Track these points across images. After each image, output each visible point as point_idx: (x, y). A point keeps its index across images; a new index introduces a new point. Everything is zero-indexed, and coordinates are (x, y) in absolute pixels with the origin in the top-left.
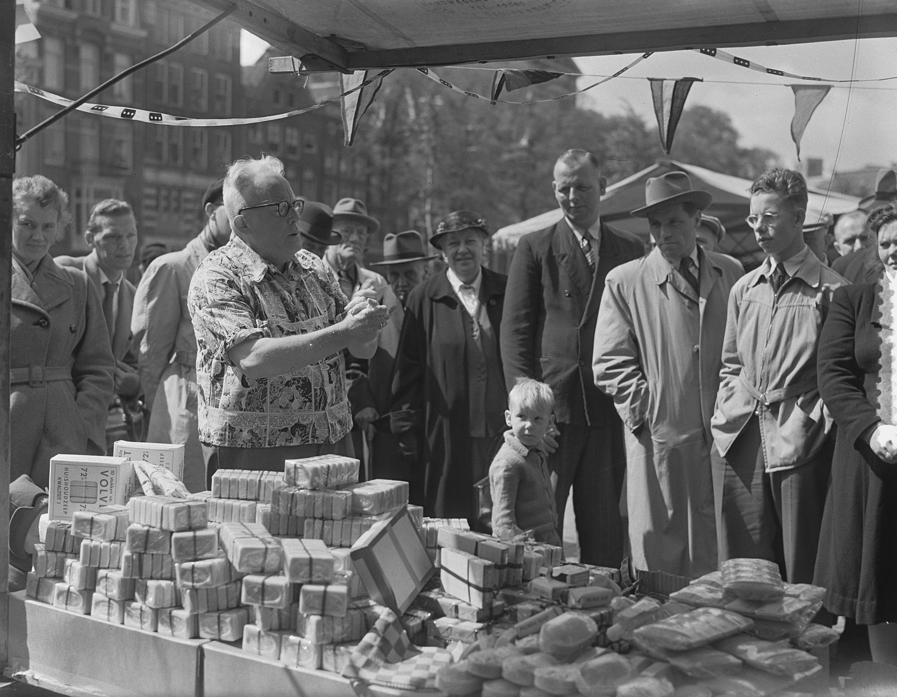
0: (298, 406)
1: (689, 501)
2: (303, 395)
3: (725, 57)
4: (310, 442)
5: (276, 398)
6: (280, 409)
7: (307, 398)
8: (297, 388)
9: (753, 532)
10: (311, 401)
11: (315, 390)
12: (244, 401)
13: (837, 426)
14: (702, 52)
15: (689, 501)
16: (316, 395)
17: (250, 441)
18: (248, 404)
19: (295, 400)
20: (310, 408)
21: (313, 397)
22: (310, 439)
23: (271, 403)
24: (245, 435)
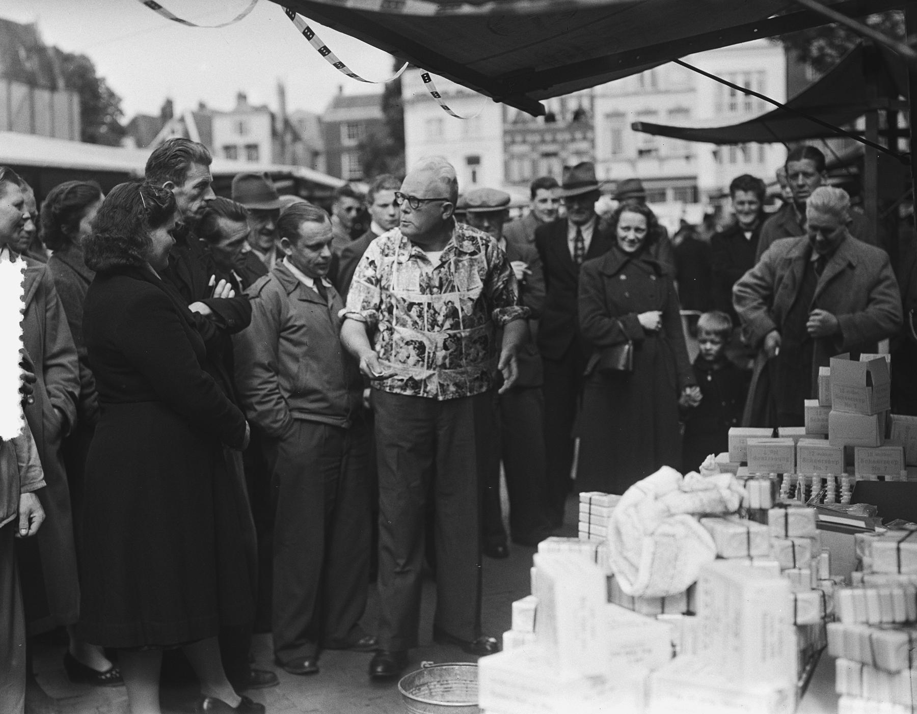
0: (413, 363)
1: (502, 472)
2: (418, 355)
3: (299, 24)
4: (421, 395)
5: (398, 353)
6: (400, 363)
7: (420, 358)
8: (414, 348)
9: (755, 304)
10: (423, 361)
11: (429, 353)
12: (447, 361)
13: (870, 372)
14: (287, 13)
15: (502, 472)
16: (429, 357)
17: (457, 392)
18: (451, 364)
19: (411, 358)
20: (423, 366)
21: (426, 358)
22: (422, 392)
23: (395, 356)
24: (452, 388)
